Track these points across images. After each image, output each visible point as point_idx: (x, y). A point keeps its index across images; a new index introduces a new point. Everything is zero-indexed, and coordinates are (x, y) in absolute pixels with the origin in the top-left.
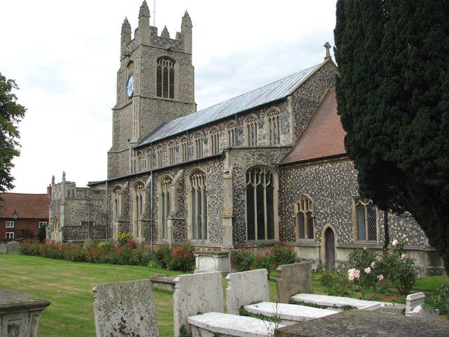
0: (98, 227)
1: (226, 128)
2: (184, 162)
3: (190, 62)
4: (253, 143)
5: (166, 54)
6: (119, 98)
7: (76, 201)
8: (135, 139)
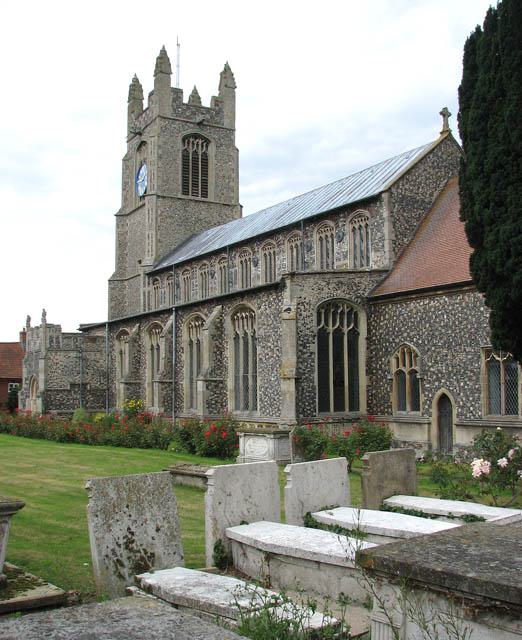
0: (94, 392)
4: (328, 265)
8: (149, 260)
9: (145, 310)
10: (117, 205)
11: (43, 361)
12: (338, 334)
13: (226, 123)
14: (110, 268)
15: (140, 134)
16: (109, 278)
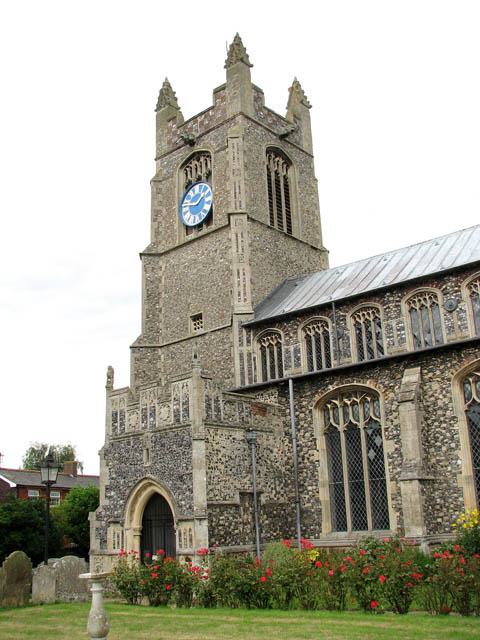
0: (269, 509)
1: (299, 331)
2: (418, 350)
3: (312, 169)
4: (370, 350)
5: (278, 144)
6: (156, 232)
7: (225, 432)
8: (243, 306)
9: (243, 382)
10: (144, 240)
11: (202, 444)
12: (352, 429)
13: (305, 147)
14: (134, 330)
15: (192, 143)
16: (131, 344)
